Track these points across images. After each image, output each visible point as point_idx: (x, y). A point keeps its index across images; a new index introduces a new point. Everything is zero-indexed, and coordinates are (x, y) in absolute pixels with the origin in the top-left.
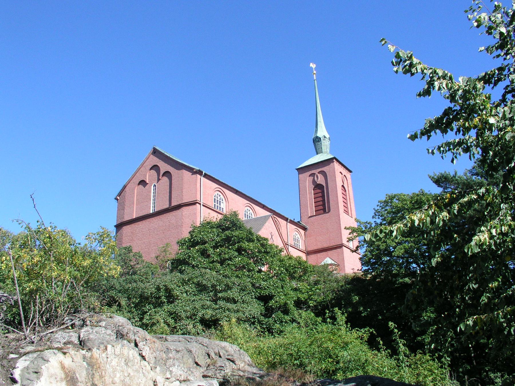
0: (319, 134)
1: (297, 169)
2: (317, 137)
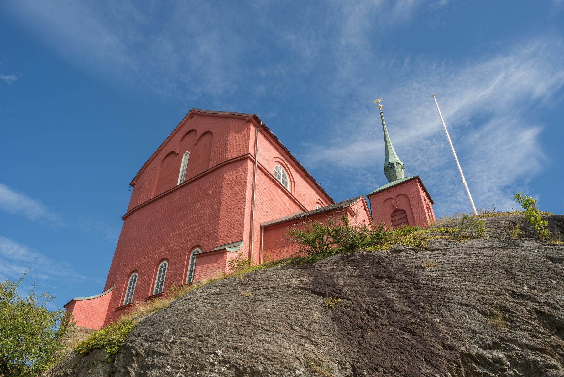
0: (391, 161)
1: (368, 196)
2: (390, 164)
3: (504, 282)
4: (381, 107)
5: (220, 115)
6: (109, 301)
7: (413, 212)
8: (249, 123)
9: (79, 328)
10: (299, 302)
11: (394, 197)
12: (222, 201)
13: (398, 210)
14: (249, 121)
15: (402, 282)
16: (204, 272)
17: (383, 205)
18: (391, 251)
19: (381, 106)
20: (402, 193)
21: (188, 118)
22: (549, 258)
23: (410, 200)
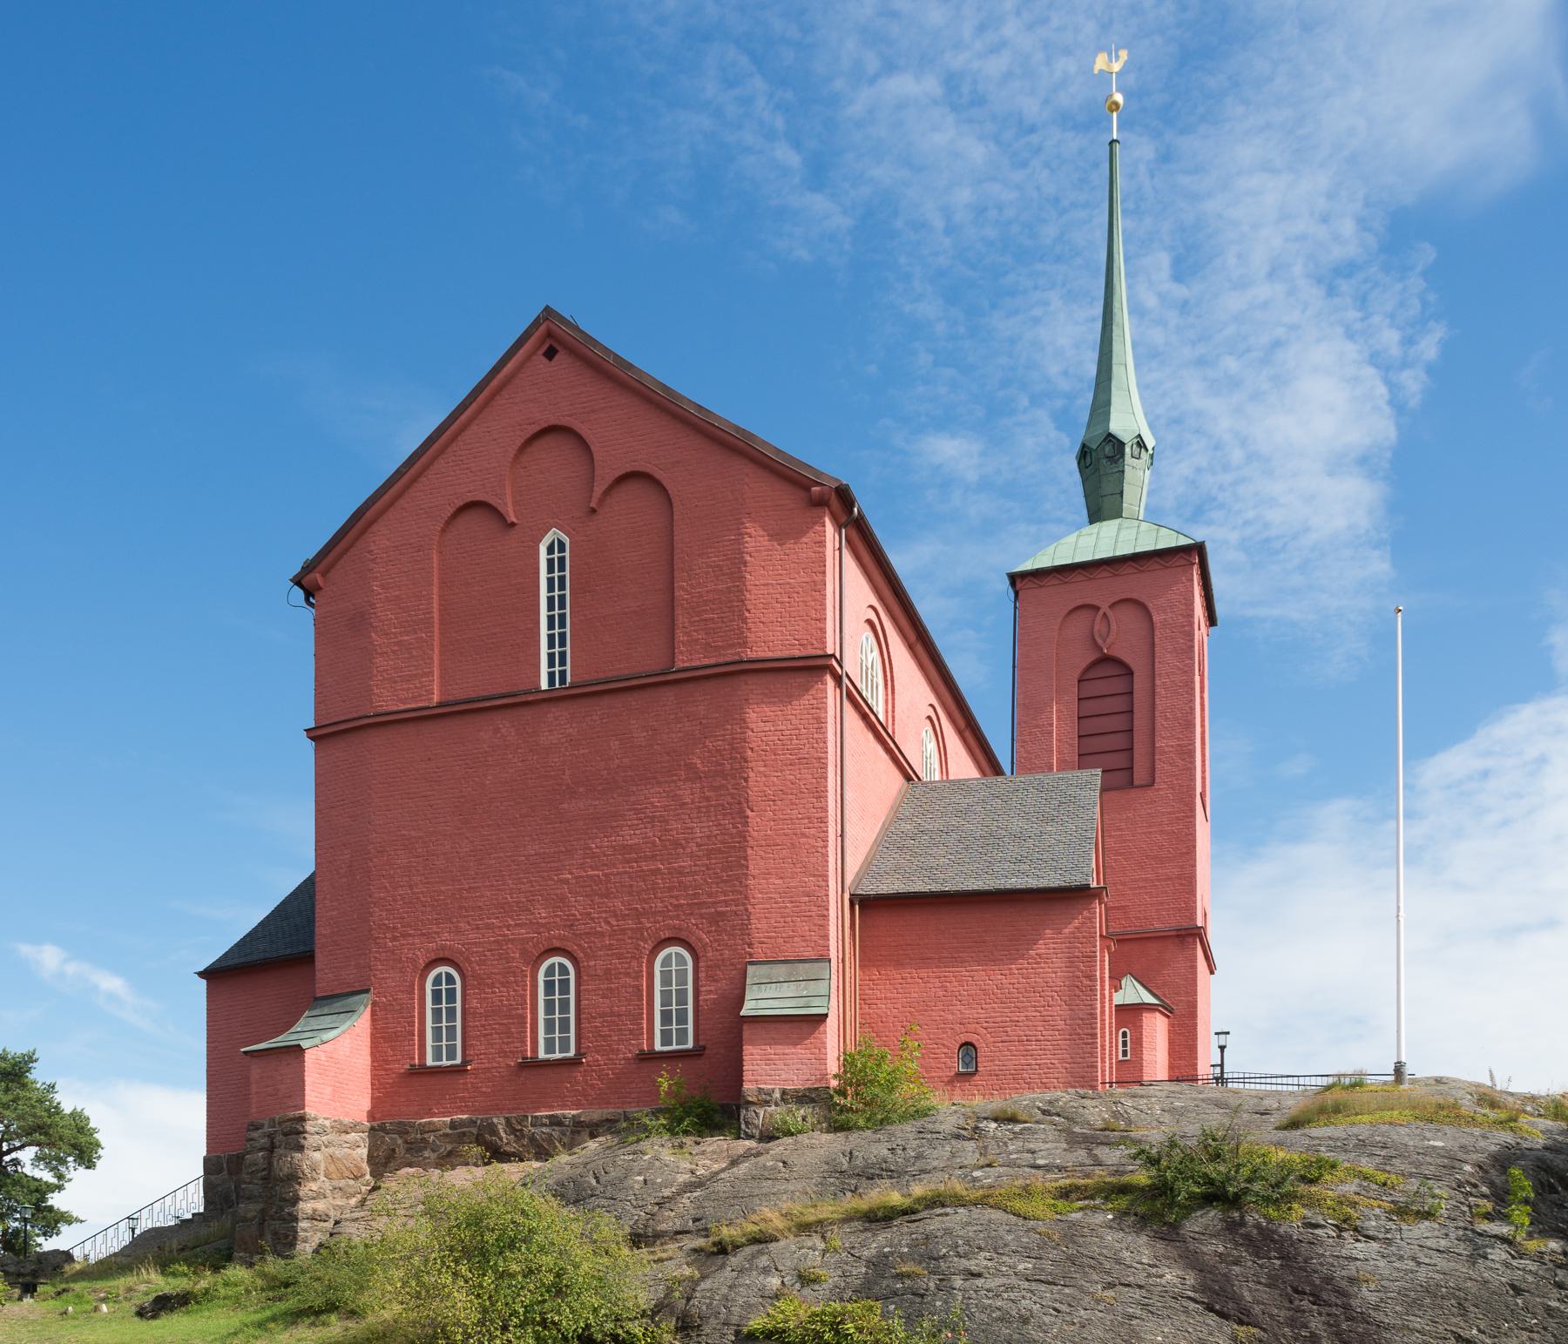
2: (1110, 438)
3: (1454, 1320)
4: (1116, 104)
5: (697, 420)
6: (369, 1040)
7: (1158, 682)
8: (818, 510)
9: (327, 1123)
10: (1199, 1329)
11: (1105, 608)
12: (749, 813)
13: (1106, 660)
14: (820, 503)
15: (1330, 1306)
16: (769, 1065)
17: (1060, 629)
18: (1303, 1224)
19: (1119, 98)
20: (1135, 596)
21: (529, 357)
22: (1513, 1287)
23: (1157, 633)
